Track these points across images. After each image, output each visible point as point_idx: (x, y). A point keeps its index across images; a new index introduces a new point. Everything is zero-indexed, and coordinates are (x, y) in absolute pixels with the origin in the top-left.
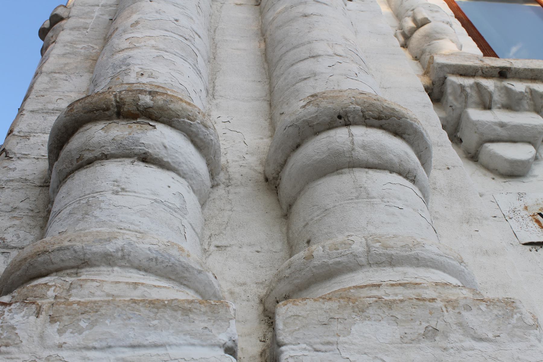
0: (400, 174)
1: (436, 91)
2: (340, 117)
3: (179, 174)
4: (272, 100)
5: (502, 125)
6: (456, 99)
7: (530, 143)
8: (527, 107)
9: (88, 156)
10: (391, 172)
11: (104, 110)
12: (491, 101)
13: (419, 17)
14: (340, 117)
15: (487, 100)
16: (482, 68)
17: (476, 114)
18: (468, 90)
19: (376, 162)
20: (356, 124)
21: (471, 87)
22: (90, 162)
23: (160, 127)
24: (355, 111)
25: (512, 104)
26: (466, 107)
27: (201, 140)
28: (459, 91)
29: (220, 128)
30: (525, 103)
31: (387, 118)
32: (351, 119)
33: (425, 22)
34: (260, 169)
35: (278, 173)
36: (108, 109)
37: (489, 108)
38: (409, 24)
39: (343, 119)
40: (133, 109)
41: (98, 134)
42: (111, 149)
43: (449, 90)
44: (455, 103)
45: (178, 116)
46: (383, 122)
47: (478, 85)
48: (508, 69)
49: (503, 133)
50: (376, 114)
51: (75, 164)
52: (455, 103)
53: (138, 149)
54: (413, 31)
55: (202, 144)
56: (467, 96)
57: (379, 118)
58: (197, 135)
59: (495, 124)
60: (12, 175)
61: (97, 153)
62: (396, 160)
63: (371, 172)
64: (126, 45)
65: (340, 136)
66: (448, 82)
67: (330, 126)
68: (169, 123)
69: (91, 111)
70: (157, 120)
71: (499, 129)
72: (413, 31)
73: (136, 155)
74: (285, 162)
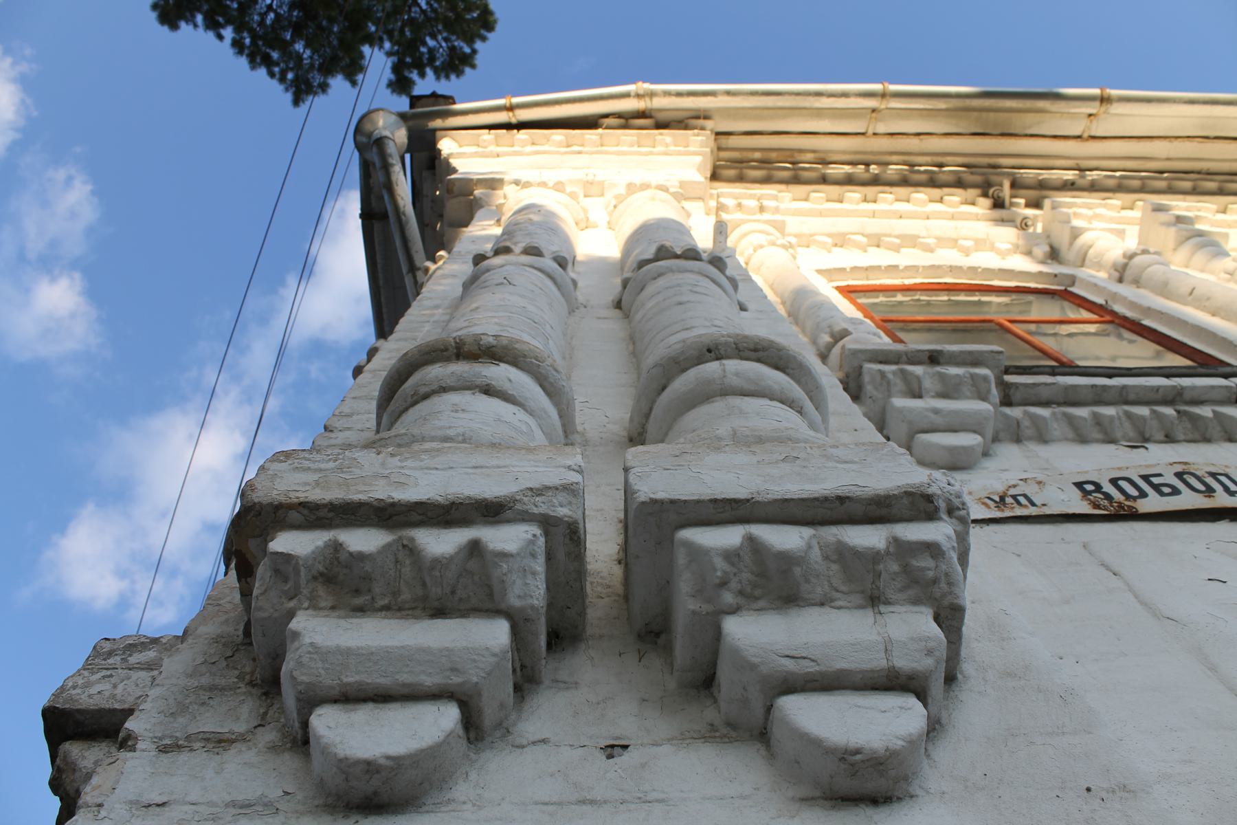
0: (782, 402)
1: (852, 385)
2: (709, 351)
3: (526, 410)
4: (635, 344)
5: (936, 411)
6: (876, 389)
7: (975, 432)
8: (968, 394)
9: (423, 390)
10: (771, 399)
11: (442, 351)
12: (920, 388)
13: (837, 328)
14: (709, 351)
15: (915, 386)
16: (906, 353)
17: (900, 402)
18: (891, 376)
19: (752, 388)
20: (728, 357)
21: (894, 373)
22: (426, 397)
23: (502, 365)
24: (726, 343)
25: (949, 391)
26: (890, 396)
27: (551, 384)
28: (878, 378)
29: (578, 406)
30: (966, 390)
31: (764, 349)
32: (722, 352)
33: (845, 334)
34: (625, 434)
35: (643, 426)
36: (446, 350)
37: (920, 397)
38: (827, 338)
39: (713, 351)
40: (474, 349)
41: (436, 372)
42: (450, 382)
43: (866, 378)
44: (875, 393)
45: (525, 356)
46: (760, 354)
47: (903, 371)
48: (940, 352)
49: (938, 420)
50: (752, 346)
51: (409, 400)
52: (875, 393)
53: (479, 381)
54: (830, 347)
55: (552, 390)
56: (889, 383)
57: (756, 350)
58: (546, 378)
59: (927, 410)
60: (333, 442)
61: (435, 387)
62: (776, 387)
63: (746, 398)
64: (466, 324)
65: (711, 368)
66: (865, 371)
67: (700, 361)
68: (515, 363)
69: (428, 353)
70: (501, 361)
71: (933, 416)
72: (830, 347)
73: (477, 386)
74: (651, 409)
